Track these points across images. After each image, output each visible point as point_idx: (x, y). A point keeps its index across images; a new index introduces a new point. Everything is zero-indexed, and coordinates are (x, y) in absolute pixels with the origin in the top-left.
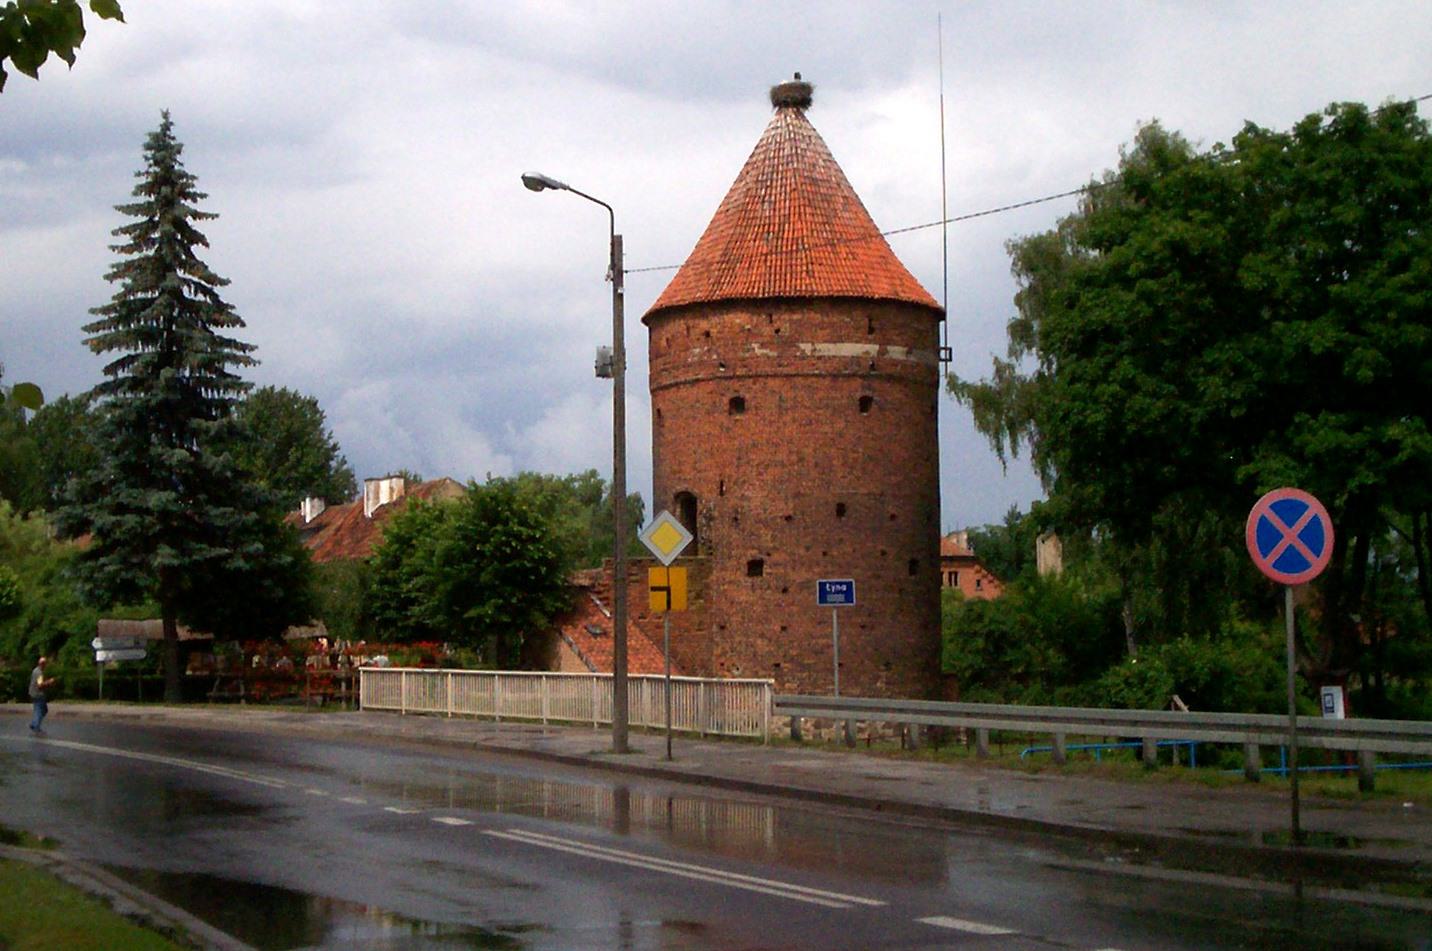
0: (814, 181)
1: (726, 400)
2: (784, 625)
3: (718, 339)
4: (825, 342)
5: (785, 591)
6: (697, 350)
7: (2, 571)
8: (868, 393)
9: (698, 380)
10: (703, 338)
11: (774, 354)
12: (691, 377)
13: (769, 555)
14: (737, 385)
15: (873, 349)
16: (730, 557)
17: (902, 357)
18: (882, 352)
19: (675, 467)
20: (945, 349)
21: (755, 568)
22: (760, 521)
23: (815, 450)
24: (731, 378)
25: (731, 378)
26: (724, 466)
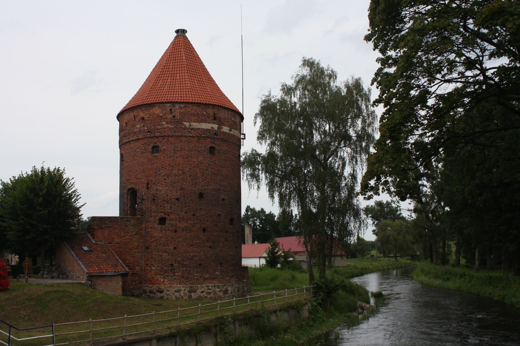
1: (150, 147)
3: (148, 121)
4: (195, 122)
5: (176, 231)
6: (139, 126)
9: (138, 139)
10: (141, 120)
12: (135, 138)
13: (169, 215)
15: (216, 127)
16: (151, 216)
19: (128, 178)
21: (162, 221)
23: (190, 169)
24: (153, 137)
25: (153, 137)
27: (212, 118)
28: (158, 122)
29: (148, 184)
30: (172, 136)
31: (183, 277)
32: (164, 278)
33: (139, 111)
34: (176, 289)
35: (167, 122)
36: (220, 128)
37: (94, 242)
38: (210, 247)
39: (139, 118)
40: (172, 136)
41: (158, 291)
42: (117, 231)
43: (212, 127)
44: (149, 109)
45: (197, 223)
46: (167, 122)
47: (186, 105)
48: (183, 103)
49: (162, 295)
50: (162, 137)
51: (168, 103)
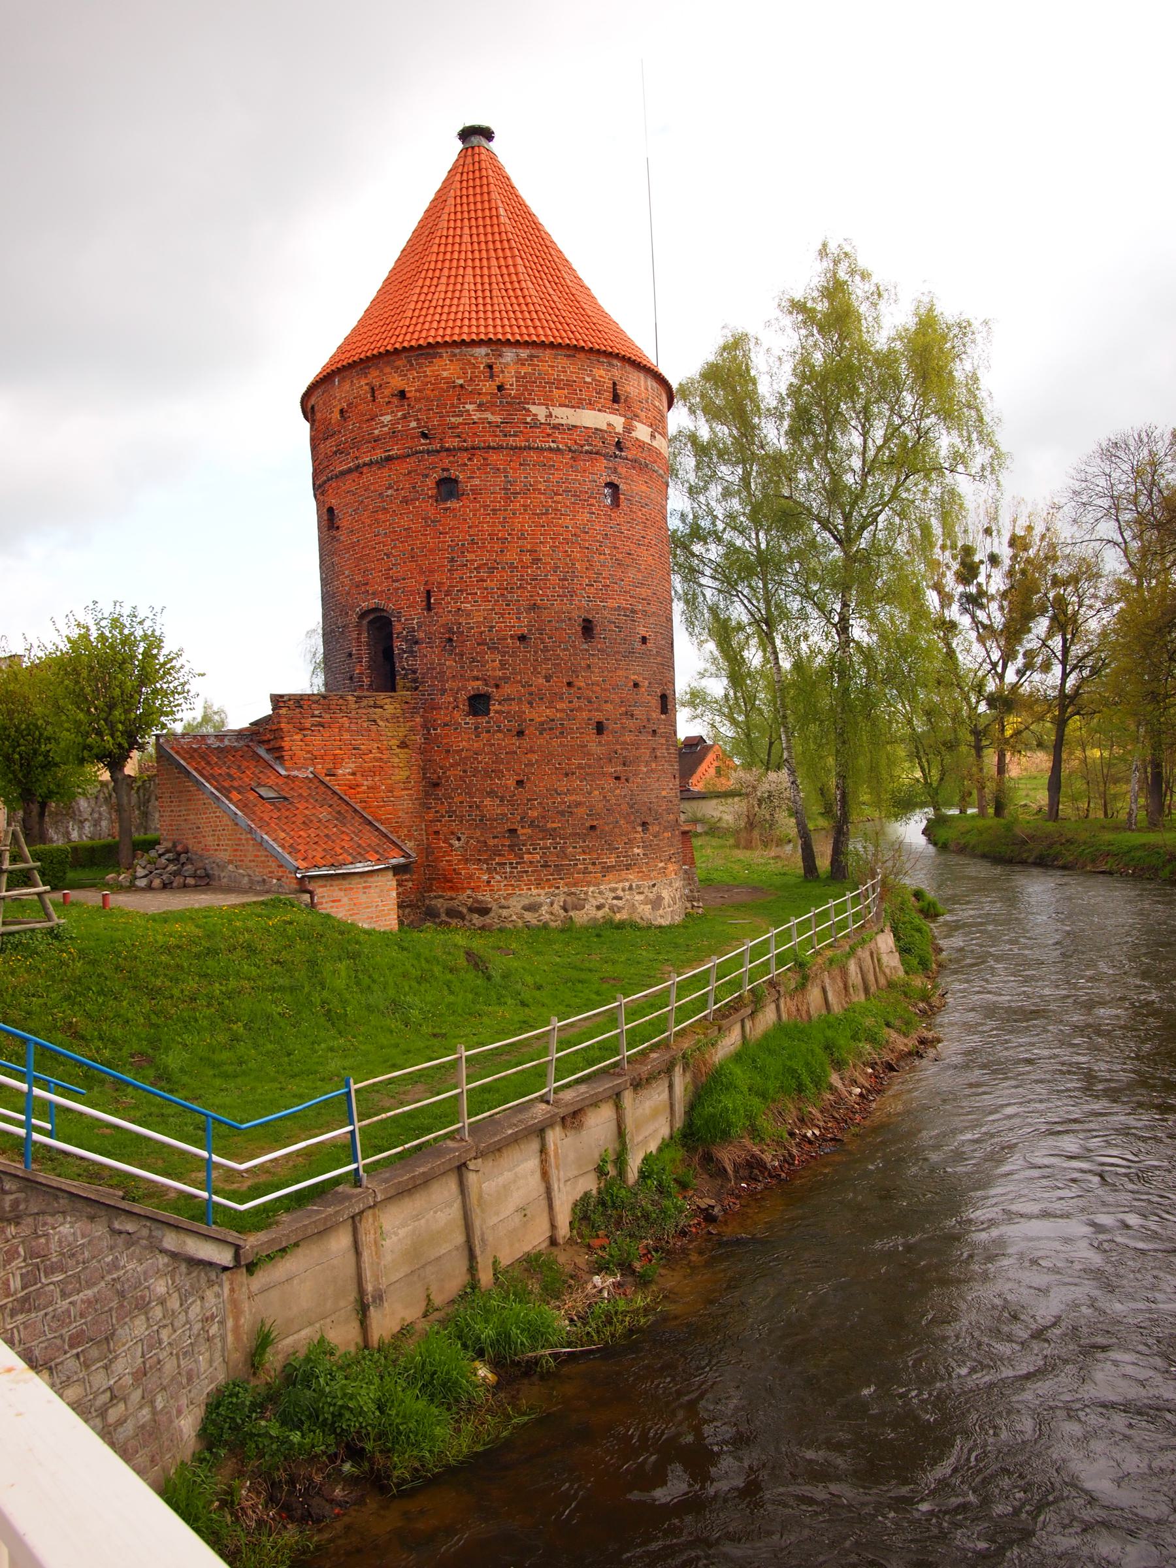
1: (430, 482)
2: (518, 778)
4: (560, 405)
5: (520, 733)
6: (387, 418)
7: (1170, 999)
9: (389, 459)
10: (395, 401)
12: (379, 454)
13: (497, 686)
15: (618, 422)
16: (443, 691)
19: (358, 578)
21: (478, 704)
22: (483, 643)
26: (432, 572)
27: (608, 395)
28: (453, 406)
29: (429, 594)
30: (498, 448)
31: (546, 866)
32: (489, 871)
33: (388, 370)
34: (527, 902)
35: (480, 406)
36: (628, 429)
37: (283, 772)
38: (618, 778)
39: (387, 392)
40: (498, 448)
41: (471, 910)
42: (346, 736)
43: (609, 425)
44: (420, 365)
45: (580, 709)
46: (480, 406)
47: (535, 352)
48: (527, 344)
49: (487, 920)
50: (466, 450)
51: (481, 343)
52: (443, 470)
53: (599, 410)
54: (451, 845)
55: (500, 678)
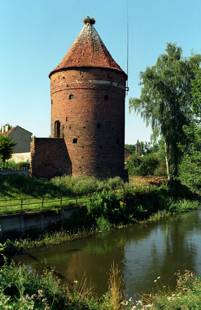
0: (123, 253)
6: (61, 82)
8: (107, 94)
11: (81, 82)
12: (59, 89)
14: (71, 91)
15: (109, 83)
17: (116, 86)
18: (111, 84)
19: (55, 114)
20: (127, 88)
36: (111, 84)
38: (104, 157)
39: (62, 77)
52: (71, 93)
53: (104, 80)
54: (69, 169)
55: (79, 136)
